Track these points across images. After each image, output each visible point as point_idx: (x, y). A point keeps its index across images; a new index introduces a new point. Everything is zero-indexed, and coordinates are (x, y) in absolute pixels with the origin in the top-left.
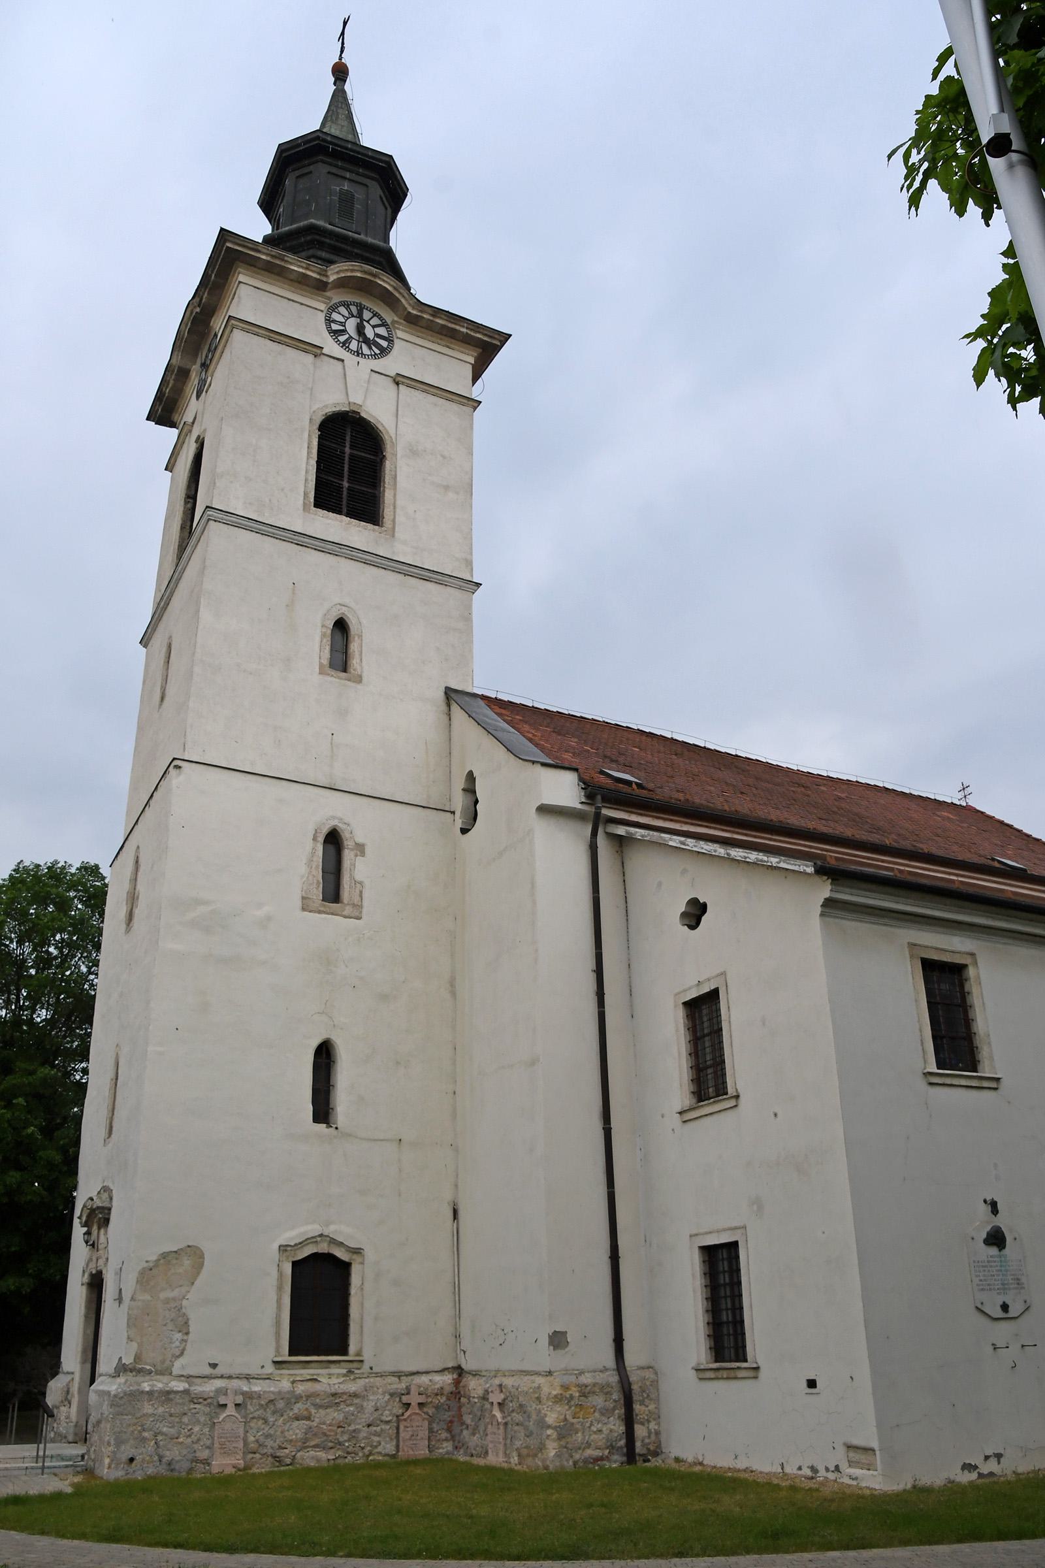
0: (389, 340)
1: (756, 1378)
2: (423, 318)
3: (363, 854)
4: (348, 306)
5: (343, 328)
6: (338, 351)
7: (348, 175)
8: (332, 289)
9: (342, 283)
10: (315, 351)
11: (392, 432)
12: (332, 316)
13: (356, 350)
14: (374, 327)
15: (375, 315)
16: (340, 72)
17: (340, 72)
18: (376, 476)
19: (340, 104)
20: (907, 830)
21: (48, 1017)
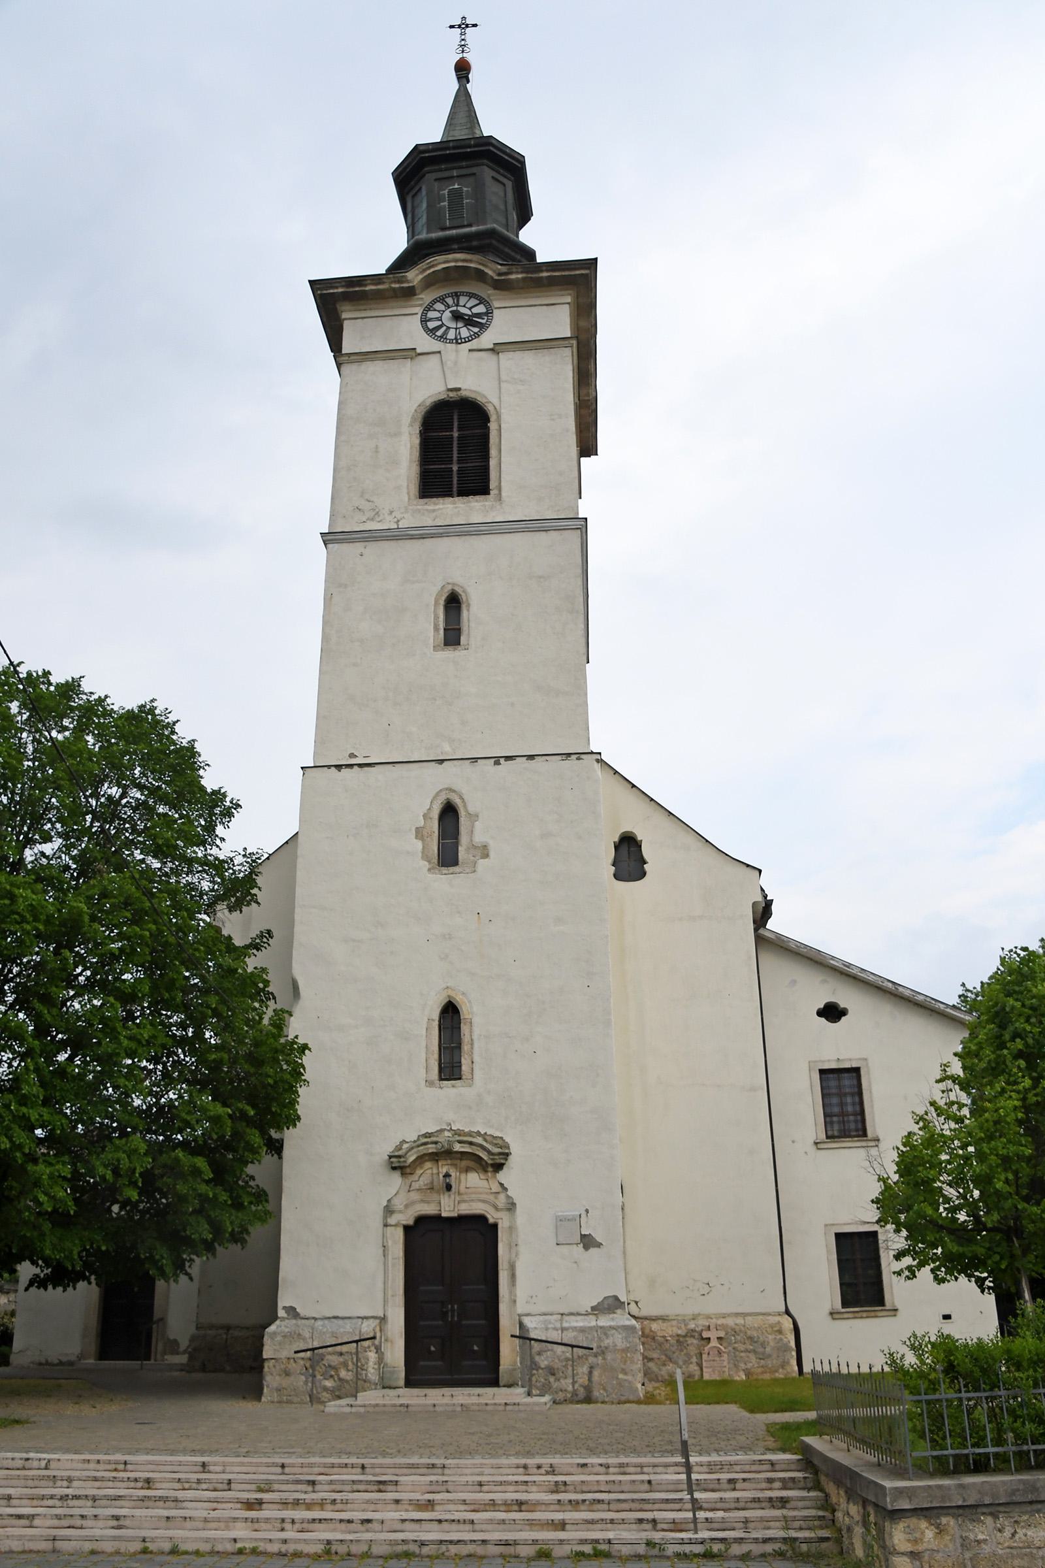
0: (489, 313)
2: (542, 277)
4: (443, 299)
5: (440, 323)
6: (436, 345)
7: (455, 173)
10: (410, 354)
11: (495, 401)
15: (471, 296)
16: (463, 69)
17: (463, 69)
18: (423, 485)
19: (463, 105)
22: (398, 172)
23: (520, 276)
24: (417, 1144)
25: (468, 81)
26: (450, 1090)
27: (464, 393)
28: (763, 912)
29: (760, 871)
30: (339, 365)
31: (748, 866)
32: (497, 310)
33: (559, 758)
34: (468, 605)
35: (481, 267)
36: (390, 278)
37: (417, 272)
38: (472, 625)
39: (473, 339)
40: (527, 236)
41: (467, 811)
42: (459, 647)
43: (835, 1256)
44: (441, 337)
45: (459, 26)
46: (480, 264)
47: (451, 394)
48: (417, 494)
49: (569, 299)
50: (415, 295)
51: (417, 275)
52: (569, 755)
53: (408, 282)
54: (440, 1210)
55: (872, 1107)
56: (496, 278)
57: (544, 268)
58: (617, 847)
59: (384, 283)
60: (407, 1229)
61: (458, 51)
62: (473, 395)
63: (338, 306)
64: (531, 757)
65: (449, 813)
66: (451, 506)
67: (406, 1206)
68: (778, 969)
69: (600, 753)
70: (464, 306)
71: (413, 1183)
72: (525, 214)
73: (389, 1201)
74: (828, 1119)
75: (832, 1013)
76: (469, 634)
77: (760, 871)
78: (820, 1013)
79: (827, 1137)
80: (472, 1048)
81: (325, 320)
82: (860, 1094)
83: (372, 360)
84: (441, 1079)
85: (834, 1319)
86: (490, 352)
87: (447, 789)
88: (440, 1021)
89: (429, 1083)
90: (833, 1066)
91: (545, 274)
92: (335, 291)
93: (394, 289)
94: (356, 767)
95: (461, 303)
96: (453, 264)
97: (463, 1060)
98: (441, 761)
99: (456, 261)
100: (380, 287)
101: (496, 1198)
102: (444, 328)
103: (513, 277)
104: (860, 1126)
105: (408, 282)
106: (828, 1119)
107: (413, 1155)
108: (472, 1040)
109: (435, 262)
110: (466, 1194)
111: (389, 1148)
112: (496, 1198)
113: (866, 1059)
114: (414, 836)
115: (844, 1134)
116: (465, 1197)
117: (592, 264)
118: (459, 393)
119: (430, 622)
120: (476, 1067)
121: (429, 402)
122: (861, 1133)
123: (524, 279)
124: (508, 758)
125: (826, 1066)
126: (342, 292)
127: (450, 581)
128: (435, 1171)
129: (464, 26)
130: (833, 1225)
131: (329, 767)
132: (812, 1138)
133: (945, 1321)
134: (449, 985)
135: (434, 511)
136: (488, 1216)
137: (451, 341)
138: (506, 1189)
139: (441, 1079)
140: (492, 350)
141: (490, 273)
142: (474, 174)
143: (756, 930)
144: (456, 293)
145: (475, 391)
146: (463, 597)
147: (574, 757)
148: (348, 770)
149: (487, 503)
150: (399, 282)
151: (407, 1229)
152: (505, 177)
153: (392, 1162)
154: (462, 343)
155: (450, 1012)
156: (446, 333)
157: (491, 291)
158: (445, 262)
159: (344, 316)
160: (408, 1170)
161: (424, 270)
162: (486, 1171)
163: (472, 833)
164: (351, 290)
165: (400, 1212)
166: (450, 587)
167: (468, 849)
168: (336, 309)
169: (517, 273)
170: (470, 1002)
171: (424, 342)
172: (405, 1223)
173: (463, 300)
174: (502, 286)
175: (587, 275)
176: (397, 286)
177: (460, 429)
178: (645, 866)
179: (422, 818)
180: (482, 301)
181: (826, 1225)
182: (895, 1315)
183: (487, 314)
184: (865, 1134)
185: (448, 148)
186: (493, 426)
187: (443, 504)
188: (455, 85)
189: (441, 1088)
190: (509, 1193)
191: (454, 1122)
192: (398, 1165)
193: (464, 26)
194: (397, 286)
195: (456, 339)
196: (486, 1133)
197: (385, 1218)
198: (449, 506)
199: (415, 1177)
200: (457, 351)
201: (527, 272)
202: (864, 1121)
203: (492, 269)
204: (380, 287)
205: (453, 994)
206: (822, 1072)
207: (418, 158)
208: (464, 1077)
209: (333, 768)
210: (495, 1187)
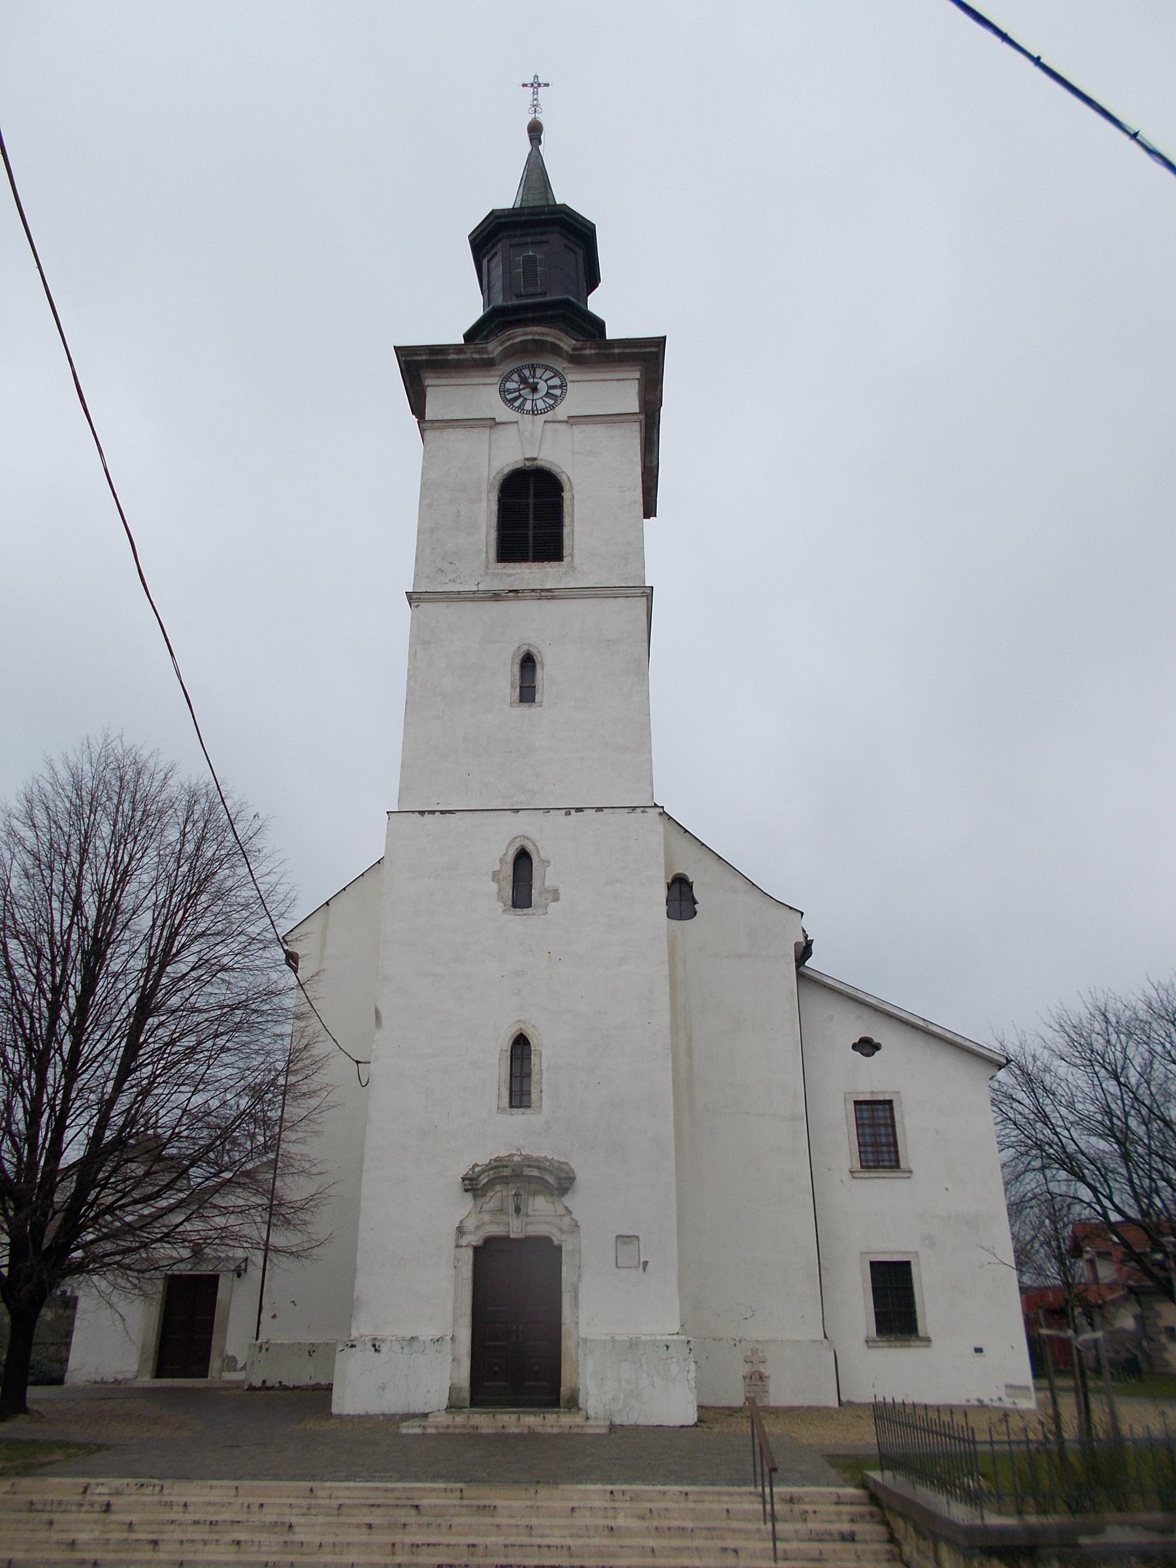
0: (563, 386)
1: (928, 1346)
3: (557, 899)
6: (512, 415)
7: (529, 240)
8: (501, 362)
9: (509, 354)
10: (493, 424)
12: (506, 386)
13: (530, 409)
14: (546, 381)
15: (547, 368)
16: (535, 131)
17: (535, 131)
20: (47, 1542)
21: (54, 1290)
22: (474, 235)
23: (593, 352)
24: (489, 1167)
25: (540, 143)
26: (519, 1117)
27: (539, 463)
28: (804, 951)
29: (802, 914)
30: (422, 431)
31: (791, 908)
32: (571, 384)
33: (627, 810)
34: (542, 666)
35: (557, 342)
36: (471, 349)
37: (497, 344)
38: (546, 684)
39: (548, 411)
40: (596, 303)
41: (539, 857)
42: (534, 705)
43: (870, 1285)
44: (519, 408)
45: (532, 85)
46: (556, 338)
47: (528, 464)
48: (495, 558)
49: (637, 375)
50: (495, 365)
51: (497, 347)
52: (634, 808)
53: (488, 353)
54: (509, 1232)
56: (571, 352)
57: (616, 345)
58: (669, 887)
59: (465, 353)
60: (476, 1249)
61: (530, 111)
62: (547, 466)
63: (421, 372)
64: (599, 809)
65: (523, 859)
66: (528, 571)
67: (477, 1228)
68: (824, 1008)
69: (663, 807)
70: (540, 378)
71: (484, 1205)
72: (593, 280)
73: (461, 1222)
74: (862, 1149)
75: (867, 1046)
76: (543, 693)
77: (802, 914)
78: (855, 1047)
79: (862, 1167)
80: (541, 1078)
81: (408, 384)
82: (893, 1126)
83: (452, 427)
84: (511, 1106)
86: (565, 424)
87: (521, 836)
88: (511, 1052)
89: (500, 1110)
90: (868, 1097)
91: (616, 351)
92: (419, 358)
93: (474, 360)
94: (438, 814)
95: (538, 375)
96: (530, 337)
97: (532, 1088)
98: (517, 810)
99: (534, 334)
100: (462, 357)
101: (561, 1221)
102: (521, 399)
103: (587, 352)
104: (893, 1157)
105: (488, 353)
107: (485, 1178)
108: (541, 1070)
109: (514, 335)
110: (533, 1216)
111: (464, 1170)
112: (561, 1221)
113: (898, 1093)
114: (491, 879)
116: (532, 1219)
117: (660, 342)
118: (535, 462)
119: (506, 679)
120: (544, 1095)
121: (506, 471)
123: (596, 354)
124: (579, 810)
126: (426, 360)
127: (526, 642)
128: (504, 1194)
129: (536, 85)
130: (868, 1253)
131: (413, 812)
133: (977, 1354)
134: (521, 1018)
135: (512, 575)
136: (554, 1238)
137: (528, 412)
138: (570, 1212)
139: (511, 1106)
140: (567, 422)
141: (566, 347)
142: (547, 242)
143: (797, 967)
144: (533, 365)
145: (550, 462)
146: (538, 659)
147: (639, 810)
148: (431, 816)
149: (561, 570)
150: (479, 353)
151: (476, 1249)
152: (577, 245)
153: (465, 1185)
154: (538, 414)
155: (521, 1044)
156: (523, 404)
157: (566, 365)
158: (522, 335)
159: (427, 382)
160: (480, 1193)
161: (503, 342)
162: (552, 1195)
163: (543, 878)
164: (434, 358)
165: (471, 1233)
166: (526, 647)
167: (540, 892)
168: (419, 375)
169: (591, 348)
170: (540, 1035)
171: (504, 413)
172: (474, 1244)
173: (539, 372)
174: (576, 360)
175: (655, 352)
176: (478, 356)
177: (535, 496)
178: (696, 906)
179: (498, 862)
180: (557, 374)
181: (861, 1253)
182: (909, 1178)
183: (561, 387)
184: (898, 1166)
185: (524, 214)
186: (566, 495)
187: (521, 568)
188: (527, 147)
189: (512, 1114)
190: (574, 1216)
191: (523, 1147)
192: (473, 1185)
193: (536, 85)
194: (478, 356)
195: (533, 410)
196: (552, 1159)
197: (457, 1239)
198: (526, 570)
199: (486, 1199)
200: (533, 422)
201: (599, 348)
203: (567, 344)
204: (462, 357)
205: (524, 1027)
207: (494, 223)
208: (533, 1105)
209: (417, 814)
210: (561, 1211)
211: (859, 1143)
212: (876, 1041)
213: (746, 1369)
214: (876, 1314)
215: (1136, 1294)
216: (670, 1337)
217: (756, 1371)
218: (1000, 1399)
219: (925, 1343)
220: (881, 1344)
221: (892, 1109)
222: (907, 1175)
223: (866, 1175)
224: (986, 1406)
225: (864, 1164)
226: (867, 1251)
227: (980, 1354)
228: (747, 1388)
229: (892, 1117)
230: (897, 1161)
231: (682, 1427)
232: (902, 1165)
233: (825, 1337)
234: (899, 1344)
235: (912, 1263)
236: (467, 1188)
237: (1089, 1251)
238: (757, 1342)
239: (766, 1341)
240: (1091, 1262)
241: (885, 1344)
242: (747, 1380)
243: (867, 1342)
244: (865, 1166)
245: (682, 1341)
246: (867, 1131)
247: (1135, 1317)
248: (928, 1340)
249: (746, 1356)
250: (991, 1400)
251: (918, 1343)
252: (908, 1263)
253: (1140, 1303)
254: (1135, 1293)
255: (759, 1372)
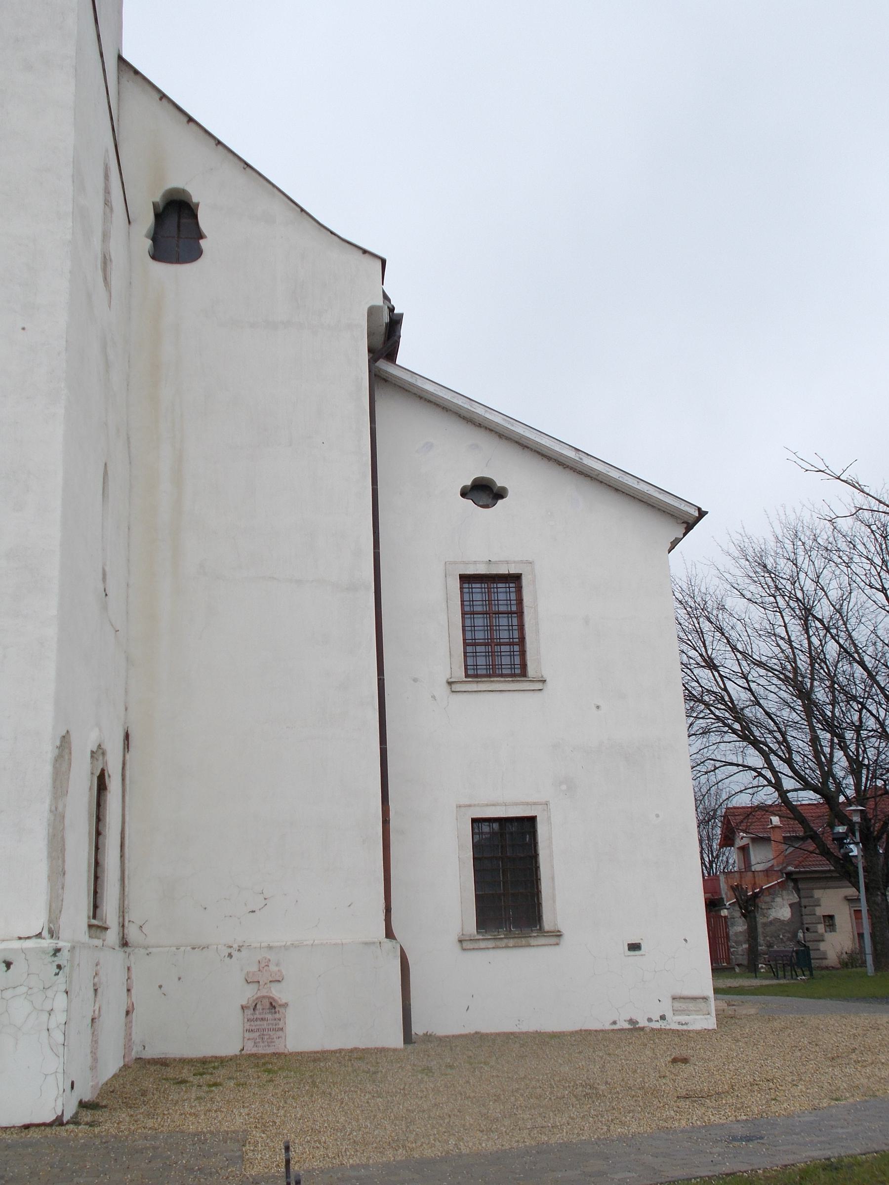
31: (365, 252)
55: (537, 632)
79: (467, 676)
82: (520, 614)
85: (464, 950)
90: (482, 570)
106: (469, 649)
115: (493, 672)
122: (518, 671)
125: (471, 571)
130: (470, 806)
132: (443, 675)
133: (632, 953)
178: (201, 241)
181: (459, 806)
182: (557, 944)
184: (524, 673)
202: (523, 653)
206: (465, 579)
211: (464, 640)
212: (499, 483)
213: (248, 994)
214: (477, 897)
215: (795, 881)
216: (17, 945)
217: (264, 997)
218: (663, 1018)
219: (553, 940)
220: (483, 944)
221: (519, 590)
222: (538, 686)
223: (474, 687)
224: (642, 1029)
225: (470, 672)
226: (468, 803)
227: (637, 953)
228: (247, 1026)
229: (520, 601)
230: (524, 666)
231: (27, 1127)
232: (531, 671)
233: (389, 934)
234: (511, 942)
235: (538, 819)
236: (718, 1013)
237: (742, 838)
238: (270, 948)
239: (286, 948)
240: (744, 850)
241: (490, 944)
242: (249, 1012)
243: (460, 941)
244: (472, 673)
245: (43, 951)
246: (479, 621)
247: (791, 906)
248: (558, 935)
249: (248, 973)
250: (650, 1020)
251: (542, 941)
252: (532, 820)
253: (798, 891)
254: (793, 880)
255: (269, 998)
